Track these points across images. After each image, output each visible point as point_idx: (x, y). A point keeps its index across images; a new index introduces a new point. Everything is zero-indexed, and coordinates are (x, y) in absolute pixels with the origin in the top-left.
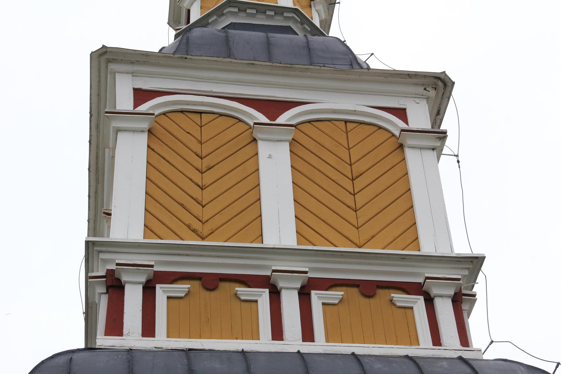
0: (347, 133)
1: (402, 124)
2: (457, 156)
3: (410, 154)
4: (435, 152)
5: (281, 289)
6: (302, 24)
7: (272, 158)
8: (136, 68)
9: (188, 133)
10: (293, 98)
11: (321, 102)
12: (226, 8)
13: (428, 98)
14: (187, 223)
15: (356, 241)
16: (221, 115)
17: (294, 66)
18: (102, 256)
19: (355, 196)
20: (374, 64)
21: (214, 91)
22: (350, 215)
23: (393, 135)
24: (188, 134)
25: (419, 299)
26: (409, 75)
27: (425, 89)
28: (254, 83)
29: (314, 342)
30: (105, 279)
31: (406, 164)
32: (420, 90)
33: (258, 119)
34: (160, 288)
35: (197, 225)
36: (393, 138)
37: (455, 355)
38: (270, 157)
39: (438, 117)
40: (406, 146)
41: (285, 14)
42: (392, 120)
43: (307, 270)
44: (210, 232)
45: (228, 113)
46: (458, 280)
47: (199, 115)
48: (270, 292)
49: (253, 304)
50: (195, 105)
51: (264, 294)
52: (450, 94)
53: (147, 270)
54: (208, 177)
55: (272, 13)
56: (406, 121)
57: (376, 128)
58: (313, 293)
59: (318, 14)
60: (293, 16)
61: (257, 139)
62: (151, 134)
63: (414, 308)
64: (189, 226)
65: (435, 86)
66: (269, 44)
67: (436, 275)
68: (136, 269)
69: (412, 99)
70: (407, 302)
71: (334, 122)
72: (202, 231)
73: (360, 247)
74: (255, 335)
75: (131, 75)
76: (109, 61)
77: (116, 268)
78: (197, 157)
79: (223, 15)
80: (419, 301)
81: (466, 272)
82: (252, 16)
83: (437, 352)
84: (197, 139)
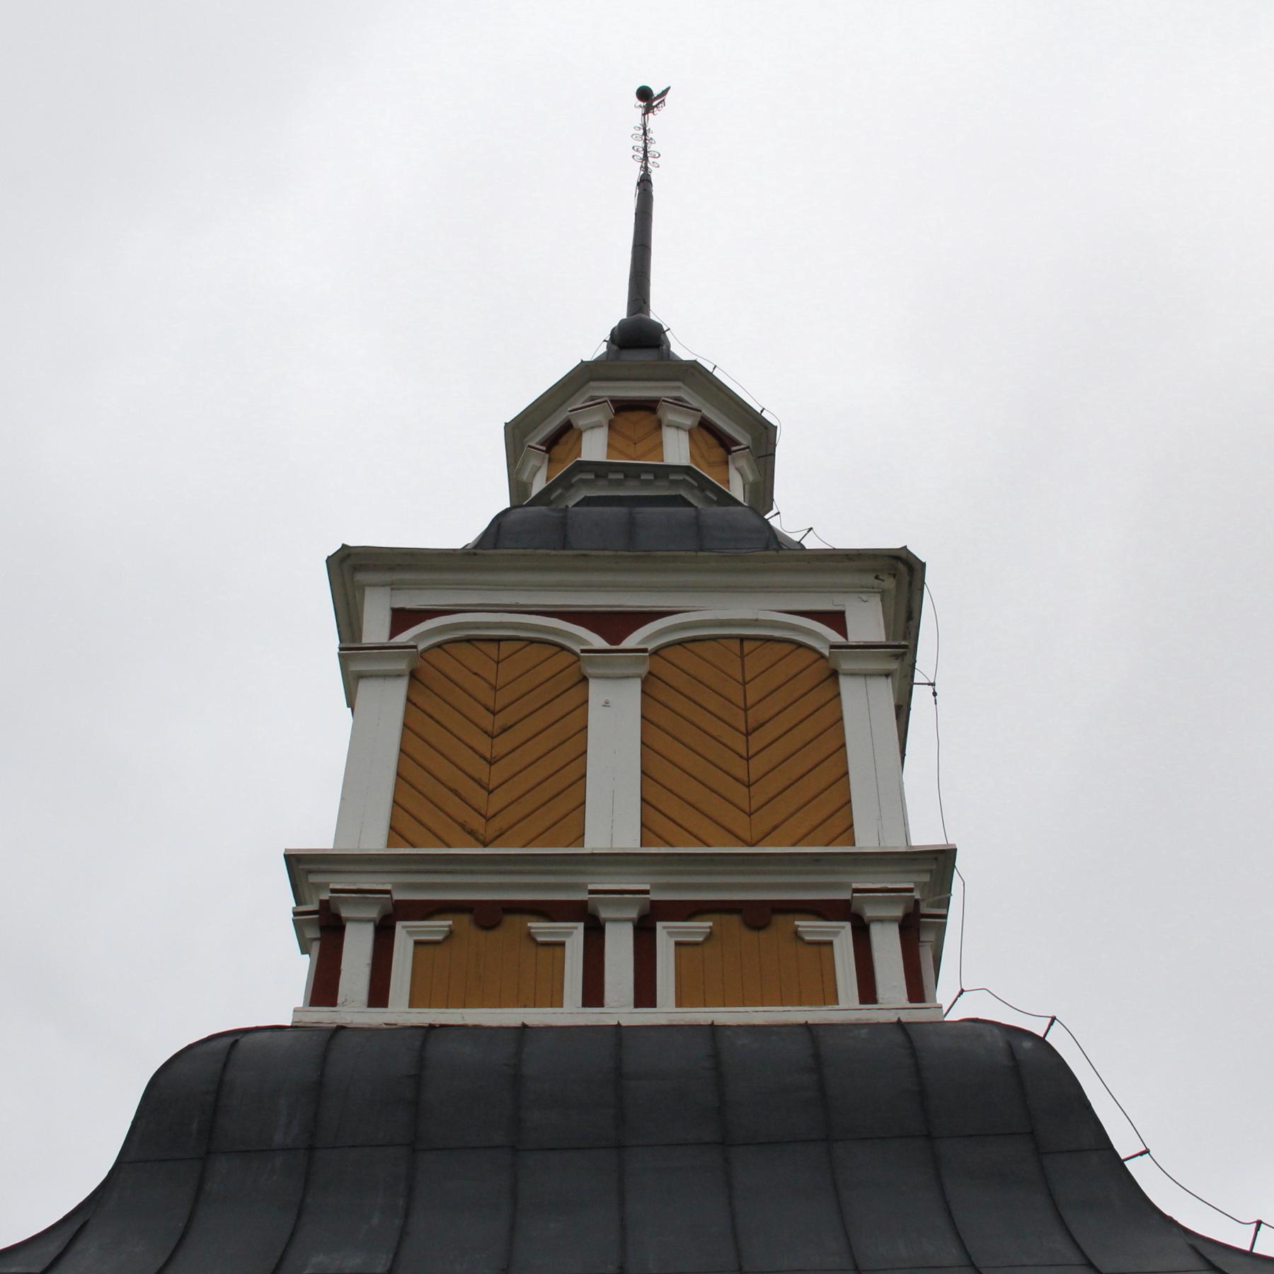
0: (742, 657)
1: (835, 637)
2: (933, 684)
3: (848, 687)
4: (890, 680)
5: (606, 920)
6: (703, 490)
7: (609, 706)
8: (397, 576)
9: (476, 674)
10: (638, 607)
11: (701, 609)
12: (574, 476)
13: (883, 592)
14: (461, 820)
15: (747, 837)
16: (532, 641)
17: (651, 553)
18: (313, 879)
19: (750, 761)
20: (810, 543)
21: (521, 603)
22: (739, 794)
23: (822, 656)
24: (475, 677)
25: (844, 927)
26: (847, 555)
27: (877, 577)
28: (588, 586)
29: (655, 1006)
30: (317, 916)
31: (840, 704)
32: (869, 579)
33: (590, 644)
34: (403, 927)
35: (477, 823)
36: (822, 661)
37: (892, 1017)
38: (606, 704)
39: (911, 623)
40: (840, 671)
41: (643, 477)
42: (817, 630)
43: (647, 887)
44: (497, 833)
45: (863, 667)
46: (910, 890)
47: (495, 645)
48: (586, 929)
49: (558, 949)
50: (478, 628)
51: (575, 931)
52: (923, 583)
53: (379, 898)
54: (503, 744)
55: (651, 477)
56: (843, 632)
57: (793, 647)
58: (660, 925)
59: (740, 476)
60: (684, 479)
61: (587, 676)
62: (417, 682)
63: (834, 943)
64: (462, 826)
65: (893, 572)
66: (631, 525)
67: (870, 884)
68: (362, 898)
69: (857, 595)
70: (822, 933)
71: (723, 641)
72: (484, 833)
73: (753, 845)
74: (555, 999)
75: (388, 589)
76: (356, 569)
77: (330, 897)
78: (487, 712)
79: (572, 486)
80: (843, 931)
81: (926, 878)
82: (618, 483)
83: (870, 1014)
84: (490, 684)
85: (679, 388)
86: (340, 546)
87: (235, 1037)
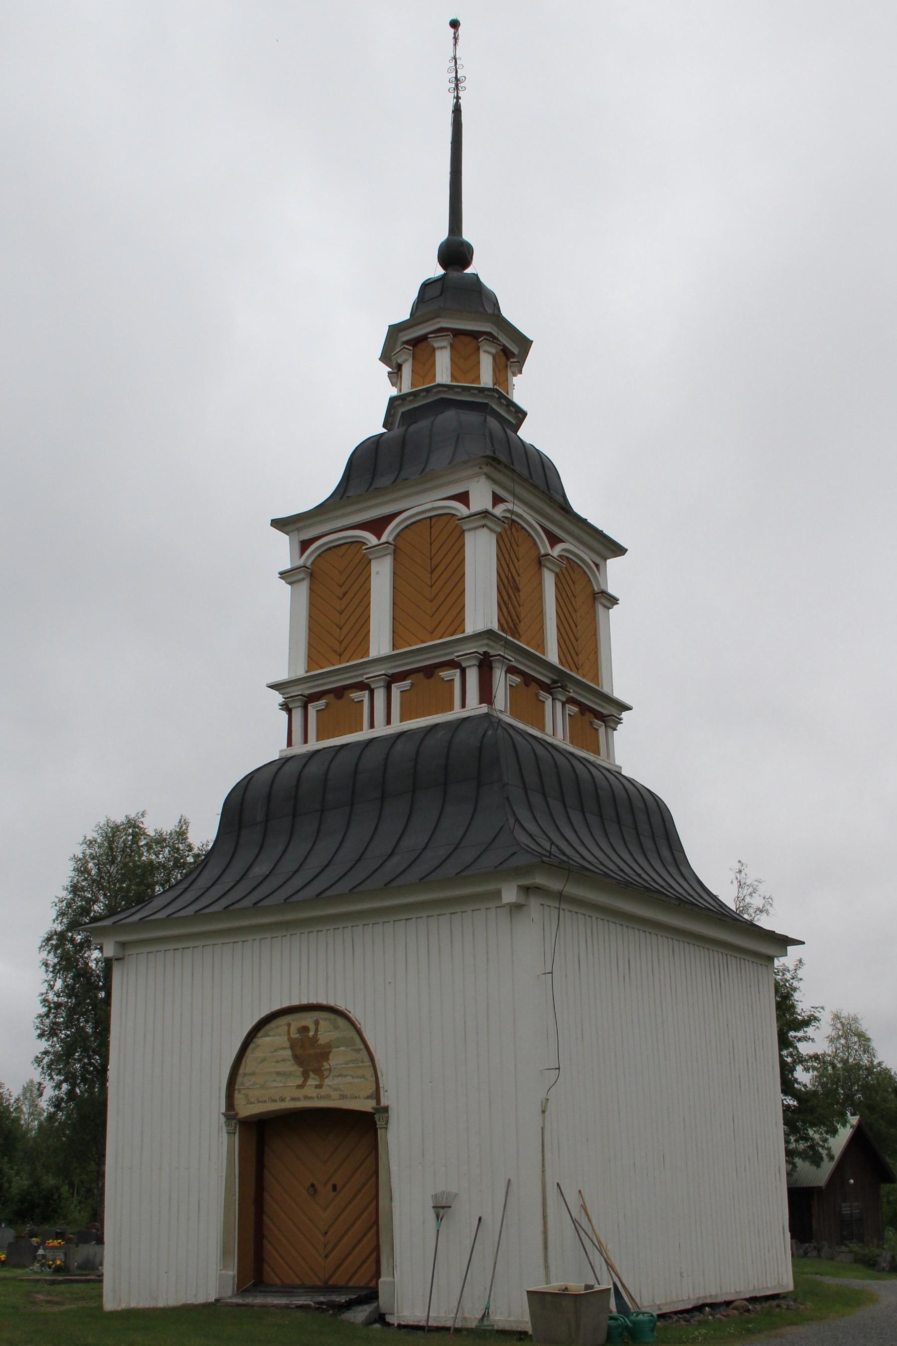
21: (345, 524)
25: (456, 672)
56: (467, 505)
74: (451, 708)
85: (439, 322)
86: (388, 327)
87: (249, 779)
